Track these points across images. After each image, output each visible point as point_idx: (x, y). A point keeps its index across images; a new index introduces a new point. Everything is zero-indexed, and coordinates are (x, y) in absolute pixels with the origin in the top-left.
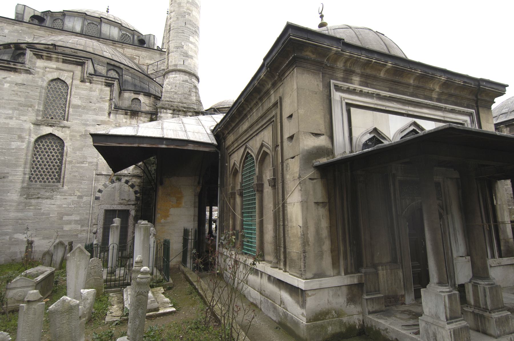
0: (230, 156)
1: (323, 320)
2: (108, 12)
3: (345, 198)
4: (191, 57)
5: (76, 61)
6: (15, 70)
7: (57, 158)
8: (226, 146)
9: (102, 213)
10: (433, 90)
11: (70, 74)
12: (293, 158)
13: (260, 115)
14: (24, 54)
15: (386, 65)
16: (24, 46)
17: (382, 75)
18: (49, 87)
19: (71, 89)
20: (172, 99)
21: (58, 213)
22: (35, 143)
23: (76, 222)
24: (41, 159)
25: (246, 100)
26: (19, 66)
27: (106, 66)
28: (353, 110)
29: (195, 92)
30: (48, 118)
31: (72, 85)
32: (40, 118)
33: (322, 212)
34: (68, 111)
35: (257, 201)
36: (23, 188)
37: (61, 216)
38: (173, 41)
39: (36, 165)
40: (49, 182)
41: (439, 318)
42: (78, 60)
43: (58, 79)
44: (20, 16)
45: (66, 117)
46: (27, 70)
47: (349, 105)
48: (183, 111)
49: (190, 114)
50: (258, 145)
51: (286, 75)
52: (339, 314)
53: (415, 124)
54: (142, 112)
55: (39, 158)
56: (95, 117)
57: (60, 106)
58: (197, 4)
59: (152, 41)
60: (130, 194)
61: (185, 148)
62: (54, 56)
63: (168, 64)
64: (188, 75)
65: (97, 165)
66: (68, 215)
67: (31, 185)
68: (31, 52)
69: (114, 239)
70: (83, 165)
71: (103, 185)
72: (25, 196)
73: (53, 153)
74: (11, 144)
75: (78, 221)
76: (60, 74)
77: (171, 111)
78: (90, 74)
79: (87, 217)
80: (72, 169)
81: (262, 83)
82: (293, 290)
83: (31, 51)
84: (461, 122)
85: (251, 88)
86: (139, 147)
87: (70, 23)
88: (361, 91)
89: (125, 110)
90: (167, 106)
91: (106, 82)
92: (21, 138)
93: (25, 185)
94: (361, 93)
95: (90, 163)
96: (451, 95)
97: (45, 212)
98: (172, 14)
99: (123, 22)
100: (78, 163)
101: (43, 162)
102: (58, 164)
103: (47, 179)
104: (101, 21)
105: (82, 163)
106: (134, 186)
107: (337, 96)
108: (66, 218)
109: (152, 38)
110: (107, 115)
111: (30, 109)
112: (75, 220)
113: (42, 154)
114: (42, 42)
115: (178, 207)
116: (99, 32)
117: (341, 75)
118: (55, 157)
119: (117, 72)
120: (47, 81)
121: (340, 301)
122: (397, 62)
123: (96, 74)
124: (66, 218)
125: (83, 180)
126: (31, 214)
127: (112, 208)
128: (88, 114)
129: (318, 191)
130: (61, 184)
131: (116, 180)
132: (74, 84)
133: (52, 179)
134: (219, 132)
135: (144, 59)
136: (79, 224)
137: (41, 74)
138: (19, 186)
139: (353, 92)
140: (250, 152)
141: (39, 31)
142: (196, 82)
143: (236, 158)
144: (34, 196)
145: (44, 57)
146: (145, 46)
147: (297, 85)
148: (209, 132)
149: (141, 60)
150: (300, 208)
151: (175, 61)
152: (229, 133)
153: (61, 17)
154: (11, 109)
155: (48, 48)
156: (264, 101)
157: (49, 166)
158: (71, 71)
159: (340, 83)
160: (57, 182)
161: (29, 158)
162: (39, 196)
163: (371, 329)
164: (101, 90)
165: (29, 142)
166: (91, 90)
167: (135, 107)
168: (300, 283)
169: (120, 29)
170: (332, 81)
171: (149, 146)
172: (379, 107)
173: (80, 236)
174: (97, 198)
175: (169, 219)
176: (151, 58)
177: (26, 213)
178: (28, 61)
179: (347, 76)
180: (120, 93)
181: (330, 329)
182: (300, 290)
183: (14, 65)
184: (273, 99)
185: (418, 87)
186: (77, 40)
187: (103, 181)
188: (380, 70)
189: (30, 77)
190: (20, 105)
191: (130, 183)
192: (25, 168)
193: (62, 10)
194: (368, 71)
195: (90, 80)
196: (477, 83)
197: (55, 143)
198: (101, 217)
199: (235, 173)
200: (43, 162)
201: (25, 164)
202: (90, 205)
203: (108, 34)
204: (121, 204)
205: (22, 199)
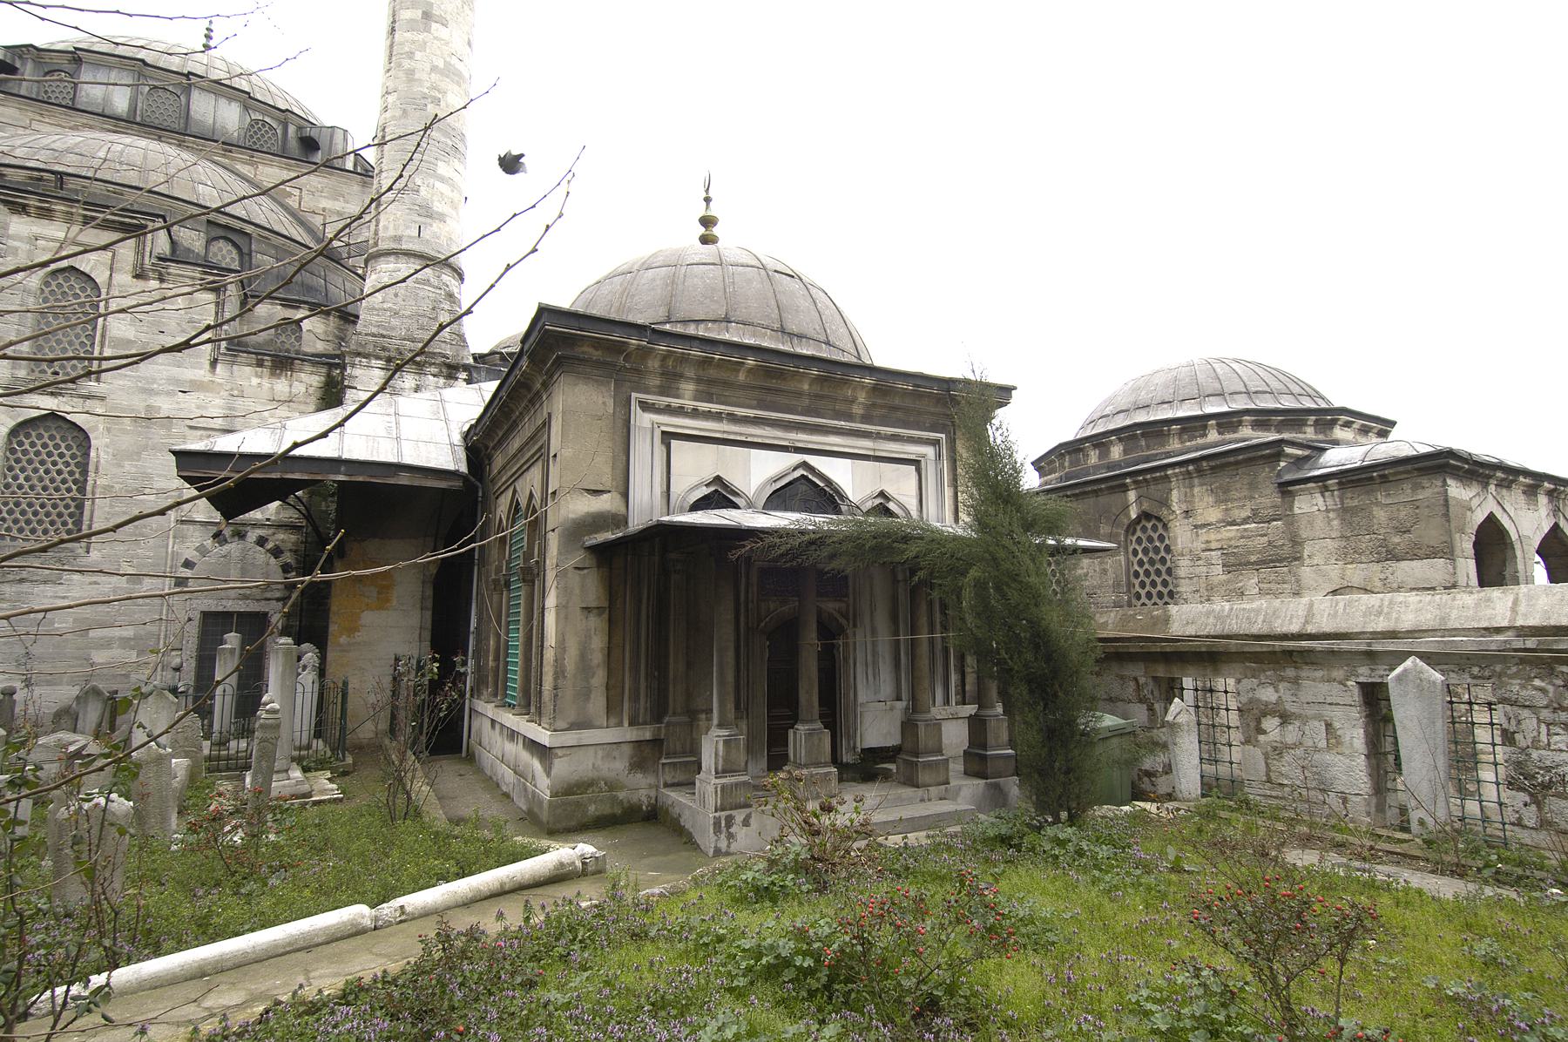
3: (645, 601)
4: (441, 218)
5: (122, 223)
9: (197, 616)
11: (111, 266)
17: (742, 377)
20: (385, 328)
23: (125, 642)
24: (27, 479)
28: (674, 443)
31: (110, 285)
33: (597, 623)
47: (668, 437)
49: (434, 370)
52: (612, 786)
53: (805, 465)
55: (22, 476)
56: (176, 372)
57: (77, 342)
58: (459, 74)
62: (60, 207)
63: (376, 233)
69: (224, 669)
71: (197, 549)
77: (381, 363)
82: (533, 746)
87: (97, 90)
88: (695, 410)
94: (695, 414)
98: (391, 99)
102: (74, 493)
109: (339, 136)
110: (207, 366)
112: (121, 639)
113: (30, 468)
115: (381, 608)
117: (655, 381)
119: (235, 245)
121: (617, 767)
122: (766, 357)
123: (177, 255)
127: (220, 609)
129: (591, 589)
132: (114, 282)
134: (481, 442)
139: (680, 411)
145: (32, 210)
148: (457, 439)
150: (563, 617)
167: (287, 341)
168: (543, 736)
169: (246, 108)
170: (634, 395)
172: (732, 437)
174: (181, 582)
175: (360, 636)
179: (669, 384)
181: (592, 808)
191: (270, 545)
195: (160, 274)
197: (63, 439)
198: (193, 630)
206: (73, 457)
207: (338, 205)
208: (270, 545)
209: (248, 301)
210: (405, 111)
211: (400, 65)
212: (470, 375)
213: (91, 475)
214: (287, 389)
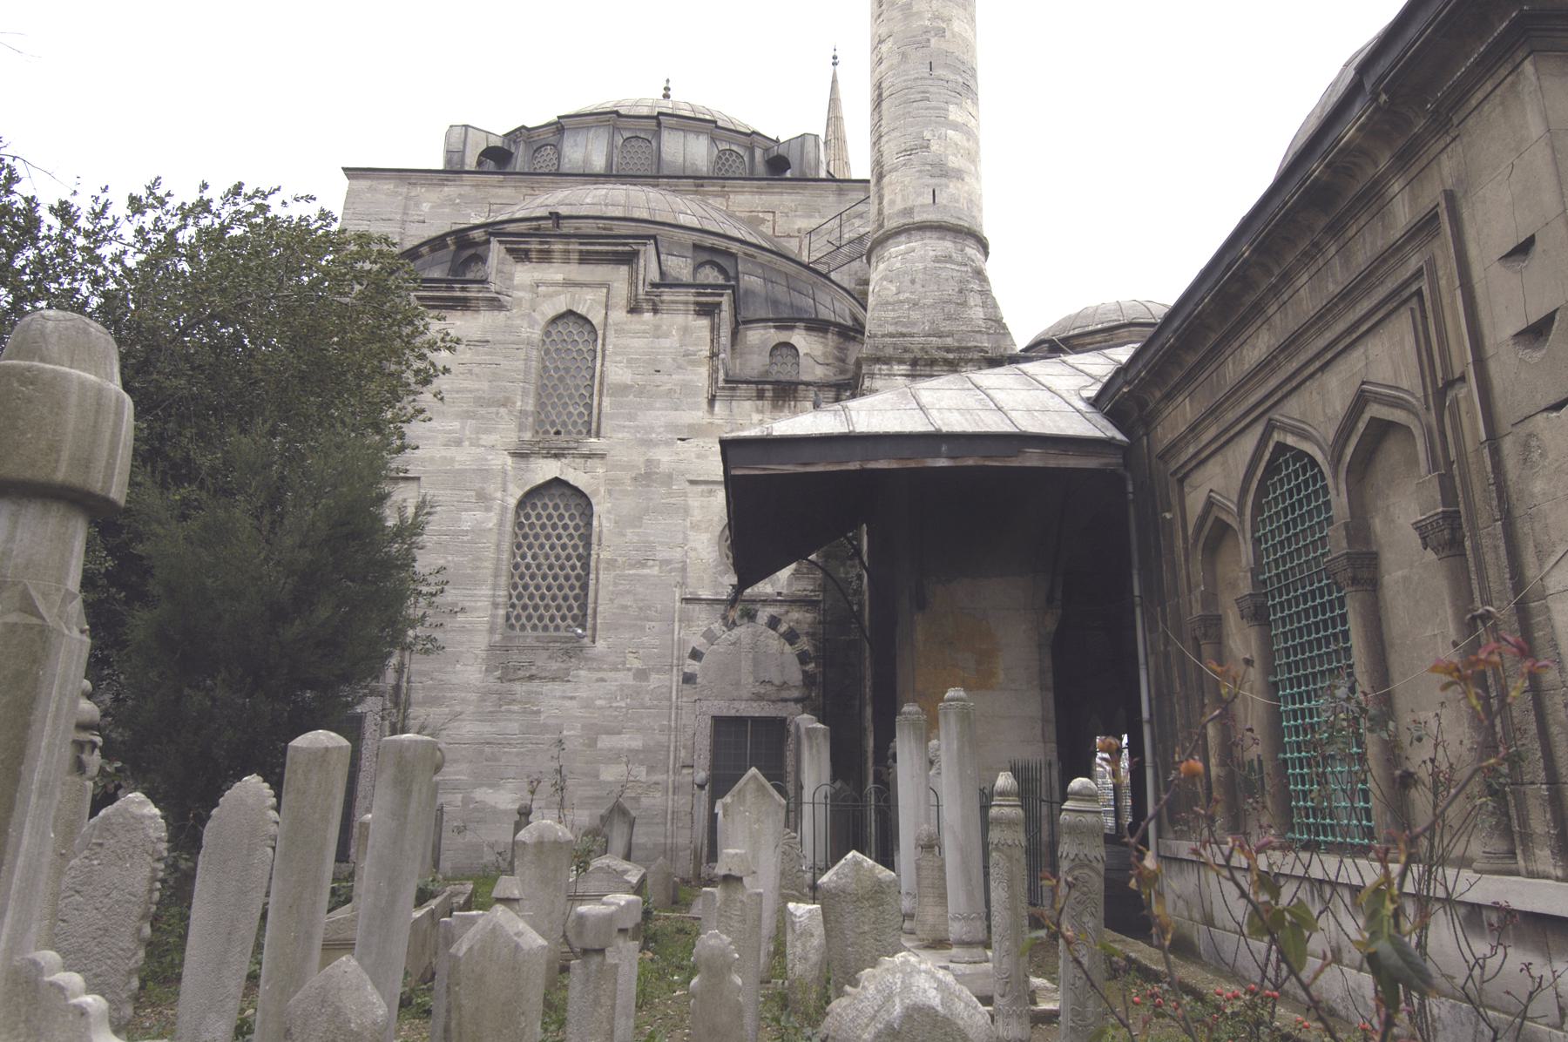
0: (1181, 481)
2: (666, 96)
4: (958, 175)
5: (615, 253)
6: (463, 304)
8: (1159, 448)
9: (706, 725)
11: (599, 293)
13: (1333, 288)
14: (481, 259)
16: (478, 235)
19: (604, 339)
21: (583, 727)
22: (517, 512)
23: (632, 756)
24: (534, 557)
25: (1262, 249)
26: (473, 292)
27: (689, 254)
29: (981, 293)
31: (605, 325)
32: (528, 436)
34: (600, 404)
35: (1354, 626)
36: (492, 647)
37: (593, 733)
39: (522, 577)
40: (557, 628)
43: (570, 313)
45: (594, 425)
46: (493, 299)
48: (947, 362)
50: (1339, 404)
51: (1474, 102)
54: (808, 384)
55: (529, 555)
57: (577, 395)
59: (812, 155)
60: (786, 663)
61: (1015, 463)
62: (558, 247)
63: (880, 212)
64: (949, 236)
65: (684, 569)
66: (610, 732)
67: (511, 639)
70: (646, 571)
71: (704, 635)
72: (498, 673)
73: (565, 540)
74: (460, 519)
75: (636, 752)
76: (573, 297)
77: (904, 368)
78: (654, 285)
79: (663, 739)
80: (615, 584)
81: (1346, 163)
85: (1291, 195)
86: (863, 471)
89: (756, 383)
90: (889, 351)
91: (697, 303)
92: (483, 498)
93: (498, 637)
98: (884, 48)
99: (717, 115)
100: (632, 566)
101: (539, 567)
104: (659, 124)
106: (797, 636)
108: (605, 742)
109: (810, 143)
110: (705, 405)
111: (502, 410)
113: (537, 543)
114: (517, 215)
118: (570, 550)
119: (722, 270)
123: (665, 282)
124: (605, 742)
126: (514, 727)
127: (732, 713)
128: (650, 407)
131: (742, 617)
132: (610, 321)
133: (564, 618)
135: (791, 220)
136: (641, 763)
137: (526, 305)
138: (481, 641)
140: (1290, 440)
141: (500, 191)
142: (980, 257)
143: (1220, 479)
144: (521, 673)
145: (533, 255)
146: (788, 174)
147: (1546, 119)
149: (780, 221)
151: (904, 199)
152: (1169, 397)
153: (552, 140)
154: (458, 416)
156: (1350, 233)
157: (555, 578)
158: (601, 285)
161: (506, 556)
162: (534, 671)
164: (685, 330)
165: (504, 509)
166: (657, 333)
167: (784, 373)
169: (713, 139)
171: (894, 465)
173: (645, 801)
174: (689, 679)
176: (810, 212)
177: (502, 724)
180: (735, 334)
183: (463, 289)
184: (1403, 213)
187: (705, 620)
189: (501, 316)
190: (480, 401)
191: (783, 628)
192: (495, 587)
193: (553, 118)
195: (654, 304)
197: (567, 508)
199: (1217, 535)
200: (539, 567)
201: (496, 576)
204: (758, 697)
205: (492, 682)
206: (577, 528)
208: (783, 628)
209: (739, 325)
210: (904, 55)
213: (595, 547)
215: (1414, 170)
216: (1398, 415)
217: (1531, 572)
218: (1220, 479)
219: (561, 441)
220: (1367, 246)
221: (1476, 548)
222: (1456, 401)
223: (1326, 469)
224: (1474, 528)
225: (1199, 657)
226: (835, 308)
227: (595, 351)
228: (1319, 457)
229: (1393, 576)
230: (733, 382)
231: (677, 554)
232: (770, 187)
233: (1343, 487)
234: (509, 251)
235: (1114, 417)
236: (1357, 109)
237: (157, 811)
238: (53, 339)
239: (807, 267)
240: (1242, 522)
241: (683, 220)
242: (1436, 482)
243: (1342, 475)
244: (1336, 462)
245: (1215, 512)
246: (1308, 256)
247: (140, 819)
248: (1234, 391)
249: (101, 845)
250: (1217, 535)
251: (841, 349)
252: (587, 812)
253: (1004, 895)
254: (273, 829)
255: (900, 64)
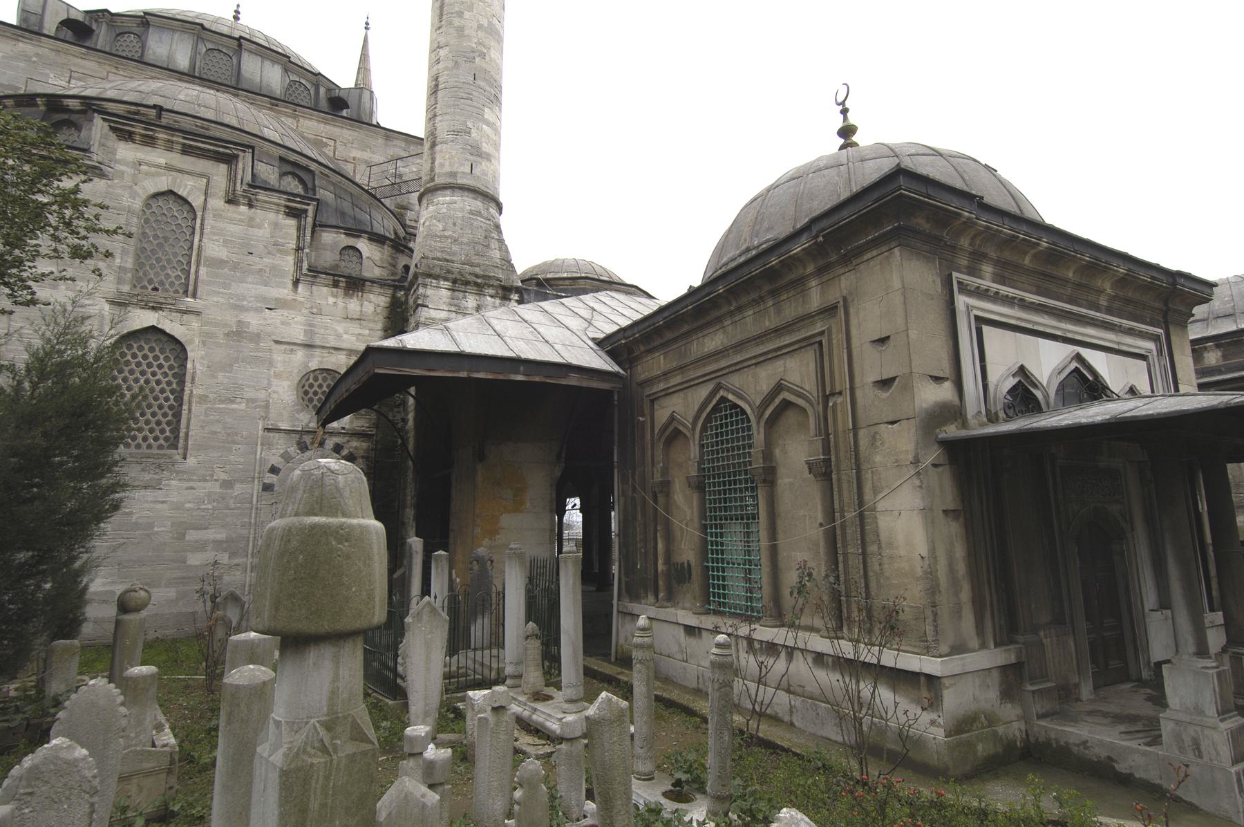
0: (652, 401)
1: (969, 731)
2: (236, 18)
7: (168, 389)
10: (1101, 292)
11: (200, 182)
12: (893, 423)
15: (1038, 244)
18: (148, 212)
19: (203, 220)
20: (448, 254)
21: (173, 524)
23: (218, 545)
28: (986, 329)
30: (144, 287)
31: (204, 208)
32: (126, 288)
33: (954, 528)
34: (197, 272)
38: (446, 117)
40: (149, 447)
41: (1201, 712)
42: (221, 150)
44: (33, 19)
45: (191, 288)
48: (476, 284)
49: (491, 291)
51: (866, 257)
53: (1078, 357)
56: (262, 290)
57: (175, 261)
61: (564, 382)
62: (162, 135)
63: (432, 169)
65: (267, 406)
68: (106, 124)
71: (282, 456)
73: (159, 376)
75: (222, 542)
76: (174, 180)
79: (244, 532)
80: (206, 415)
83: (104, 120)
84: (1142, 352)
86: (469, 379)
90: (437, 271)
91: (287, 207)
94: (997, 298)
95: (249, 401)
96: (1128, 301)
97: (141, 521)
98: (442, 53)
100: (222, 402)
103: (145, 439)
104: (240, 45)
105: (232, 402)
107: (961, 301)
108: (192, 535)
110: (290, 286)
112: (215, 541)
116: (235, 73)
117: (964, 262)
119: (301, 181)
120: (144, 197)
121: (989, 697)
123: (256, 184)
124: (192, 535)
125: (234, 442)
129: (945, 491)
130: (180, 451)
132: (209, 206)
133: (156, 439)
140: (730, 397)
141: (83, 62)
145: (137, 138)
146: (344, 113)
149: (340, 148)
151: (451, 165)
152: (650, 351)
155: (137, 113)
158: (202, 175)
159: (966, 278)
160: (169, 448)
163: (1048, 744)
164: (276, 225)
166: (251, 223)
167: (350, 268)
169: (286, 70)
171: (490, 377)
173: (226, 579)
174: (267, 488)
178: (97, 144)
180: (313, 232)
181: (980, 748)
182: (922, 679)
184: (815, 299)
185: (1079, 286)
186: (195, 93)
187: (283, 444)
188: (1025, 253)
191: (345, 452)
194: (1007, 255)
195: (250, 200)
196: (1171, 280)
197: (162, 351)
202: (251, 502)
203: (258, 80)
207: (366, 155)
208: (345, 452)
211: (451, 23)
212: (521, 296)
214: (358, 308)
215: (825, 279)
216: (800, 402)
217: (868, 495)
218: (683, 406)
219: (159, 296)
220: (791, 310)
221: (839, 480)
222: (835, 404)
223: (752, 418)
224: (838, 470)
225: (656, 502)
226: (385, 224)
227: (194, 229)
228: (749, 411)
229: (783, 481)
230: (314, 271)
231: (262, 395)
232: (333, 120)
233: (762, 430)
234: (111, 128)
235: (613, 354)
236: (804, 239)
237: (85, 752)
238: (347, 494)
239: (367, 191)
240: (693, 434)
241: (268, 133)
242: (820, 443)
243: (762, 424)
244: (759, 417)
245: (675, 424)
246: (756, 302)
247: (74, 763)
248: (697, 361)
249: (31, 794)
250: (673, 435)
251: (394, 258)
252: (173, 589)
253: (644, 689)
254: (124, 722)
255: (453, 68)
